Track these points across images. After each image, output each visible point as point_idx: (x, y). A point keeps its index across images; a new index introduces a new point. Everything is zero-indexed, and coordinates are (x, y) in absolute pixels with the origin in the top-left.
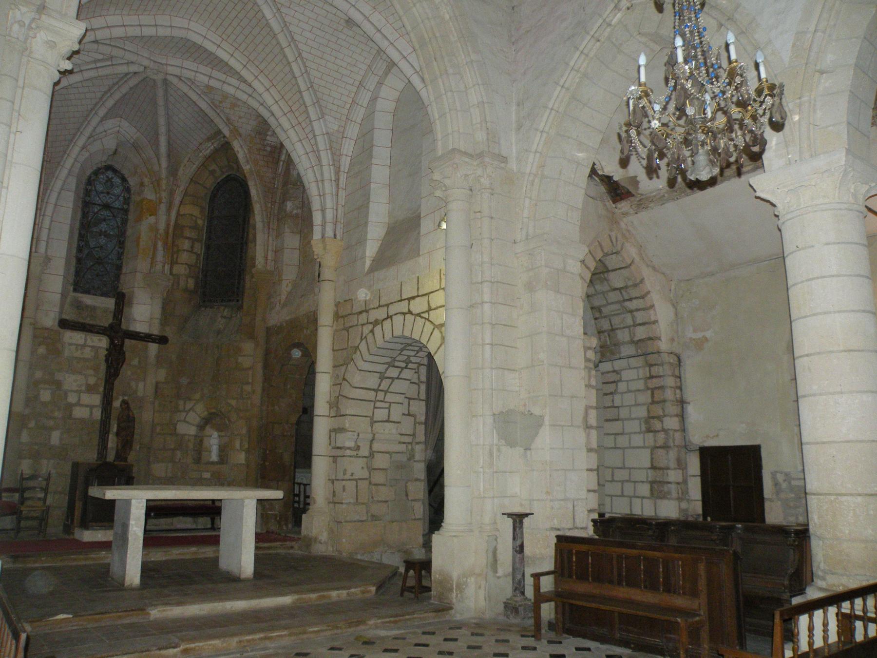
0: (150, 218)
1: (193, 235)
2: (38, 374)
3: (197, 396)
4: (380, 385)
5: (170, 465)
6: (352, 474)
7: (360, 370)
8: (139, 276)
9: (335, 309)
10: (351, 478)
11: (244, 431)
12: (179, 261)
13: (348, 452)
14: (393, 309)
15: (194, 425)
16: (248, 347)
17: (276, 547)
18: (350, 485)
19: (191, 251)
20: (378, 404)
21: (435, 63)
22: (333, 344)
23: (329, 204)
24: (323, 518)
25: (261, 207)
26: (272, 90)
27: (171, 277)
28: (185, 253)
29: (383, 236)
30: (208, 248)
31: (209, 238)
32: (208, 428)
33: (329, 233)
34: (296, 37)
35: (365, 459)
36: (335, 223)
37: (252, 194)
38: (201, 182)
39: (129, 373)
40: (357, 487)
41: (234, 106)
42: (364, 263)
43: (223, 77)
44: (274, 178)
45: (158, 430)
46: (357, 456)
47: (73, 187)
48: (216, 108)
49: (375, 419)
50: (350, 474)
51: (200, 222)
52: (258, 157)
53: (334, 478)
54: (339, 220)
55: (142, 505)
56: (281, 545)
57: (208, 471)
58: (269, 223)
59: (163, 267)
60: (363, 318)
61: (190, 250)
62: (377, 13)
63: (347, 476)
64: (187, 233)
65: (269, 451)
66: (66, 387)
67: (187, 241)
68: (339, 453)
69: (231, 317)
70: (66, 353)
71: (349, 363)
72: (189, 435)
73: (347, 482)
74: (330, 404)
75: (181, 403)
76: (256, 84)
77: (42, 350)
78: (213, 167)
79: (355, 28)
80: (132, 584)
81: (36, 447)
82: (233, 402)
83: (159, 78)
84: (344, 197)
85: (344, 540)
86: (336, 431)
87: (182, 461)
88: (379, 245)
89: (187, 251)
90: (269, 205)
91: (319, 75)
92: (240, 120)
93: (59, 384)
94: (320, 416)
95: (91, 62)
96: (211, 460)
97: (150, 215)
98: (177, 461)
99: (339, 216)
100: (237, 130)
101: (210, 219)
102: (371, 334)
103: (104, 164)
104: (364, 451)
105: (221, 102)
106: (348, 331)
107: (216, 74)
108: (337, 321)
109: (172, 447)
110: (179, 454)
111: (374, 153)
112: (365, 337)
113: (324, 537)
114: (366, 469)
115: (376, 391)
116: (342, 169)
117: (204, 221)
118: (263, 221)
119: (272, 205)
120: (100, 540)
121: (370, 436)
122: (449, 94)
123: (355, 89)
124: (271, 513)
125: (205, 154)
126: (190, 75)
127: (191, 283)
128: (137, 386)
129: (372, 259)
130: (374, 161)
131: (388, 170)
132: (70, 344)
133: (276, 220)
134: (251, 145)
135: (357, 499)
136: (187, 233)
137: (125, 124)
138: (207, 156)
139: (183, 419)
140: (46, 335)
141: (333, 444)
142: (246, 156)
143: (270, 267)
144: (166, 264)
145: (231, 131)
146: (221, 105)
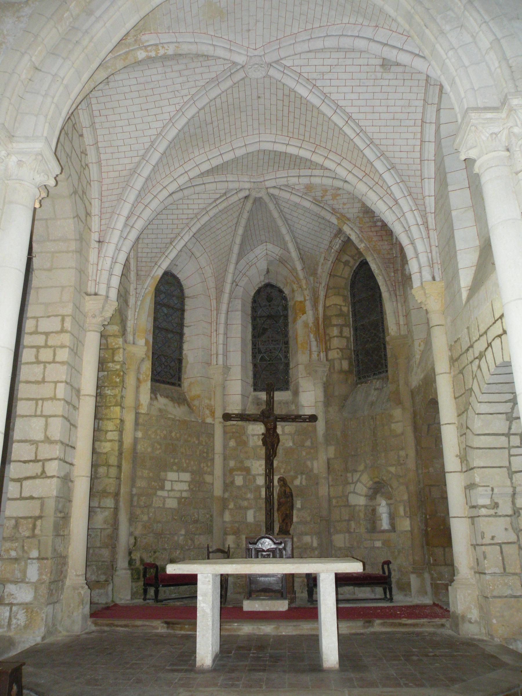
0: (302, 316)
1: (340, 321)
2: (232, 463)
3: (361, 467)
4: (510, 428)
5: (347, 535)
6: (493, 538)
7: (478, 414)
8: (301, 368)
9: (450, 354)
10: (492, 542)
11: (406, 497)
12: (332, 348)
13: (483, 511)
14: (491, 334)
15: (362, 495)
16: (397, 412)
17: (422, 625)
18: (493, 552)
19: (341, 336)
20: (513, 451)
21: (427, 31)
22: (454, 391)
23: (420, 247)
24: (470, 592)
25: (384, 278)
26: (345, 163)
27: (328, 363)
28: (335, 338)
29: (476, 262)
30: (356, 329)
31: (355, 321)
32: (378, 497)
33: (427, 276)
34: (341, 103)
35: (508, 519)
36: (431, 266)
37: (373, 269)
38: (339, 274)
39: (304, 453)
40: (502, 552)
41: (335, 196)
42: (461, 296)
43: (308, 172)
44: (391, 249)
45: (334, 501)
46: (496, 515)
47: (239, 307)
48: (320, 202)
49: (513, 469)
50: (490, 538)
51: (345, 309)
52: (371, 234)
53: (475, 543)
54: (435, 261)
55: (208, 580)
56: (429, 622)
57: (379, 540)
58: (395, 290)
59: (319, 355)
60: (470, 356)
61: (340, 335)
62: (380, 29)
63: (487, 540)
64: (335, 321)
65: (429, 515)
66: (254, 472)
67: (335, 328)
68: (474, 512)
69: (383, 387)
70: (251, 444)
71: (468, 409)
72: (359, 506)
73: (486, 547)
74: (460, 458)
75: (349, 475)
76: (328, 164)
77: (232, 443)
78: (345, 258)
79: (393, 68)
80: (203, 665)
81: (236, 525)
82: (392, 469)
83: (262, 194)
84: (436, 237)
85: (494, 621)
86: (470, 487)
87: (356, 531)
88: (473, 272)
89: (337, 337)
90: (393, 274)
91: (376, 129)
92: (345, 207)
93: (247, 470)
94: (451, 472)
95: (213, 202)
96: (382, 528)
97: (303, 314)
98: (352, 531)
99: (434, 258)
100: (344, 216)
101: (354, 304)
102: (479, 371)
103: (263, 283)
104: (506, 508)
105: (322, 197)
106: (462, 374)
107: (303, 172)
108: (454, 366)
109: (347, 518)
110: (353, 524)
111: (449, 180)
112: (476, 376)
113: (474, 614)
114: (510, 530)
115: (508, 435)
116: (428, 210)
117: (348, 307)
118: (389, 290)
119: (395, 274)
120: (258, 610)
121: (510, 490)
122: (451, 53)
123: (419, 129)
124: (441, 582)
125: (335, 249)
126: (283, 181)
127: (345, 365)
128: (312, 464)
129: (469, 288)
130: (450, 188)
131: (468, 191)
132: (253, 435)
133: (401, 287)
134: (361, 225)
135: (504, 569)
136: (335, 321)
137: (270, 246)
138: (339, 251)
139: (352, 490)
140: (234, 430)
141: (469, 504)
142: (359, 237)
143: (404, 331)
144: (321, 352)
145: (338, 219)
146: (323, 199)
